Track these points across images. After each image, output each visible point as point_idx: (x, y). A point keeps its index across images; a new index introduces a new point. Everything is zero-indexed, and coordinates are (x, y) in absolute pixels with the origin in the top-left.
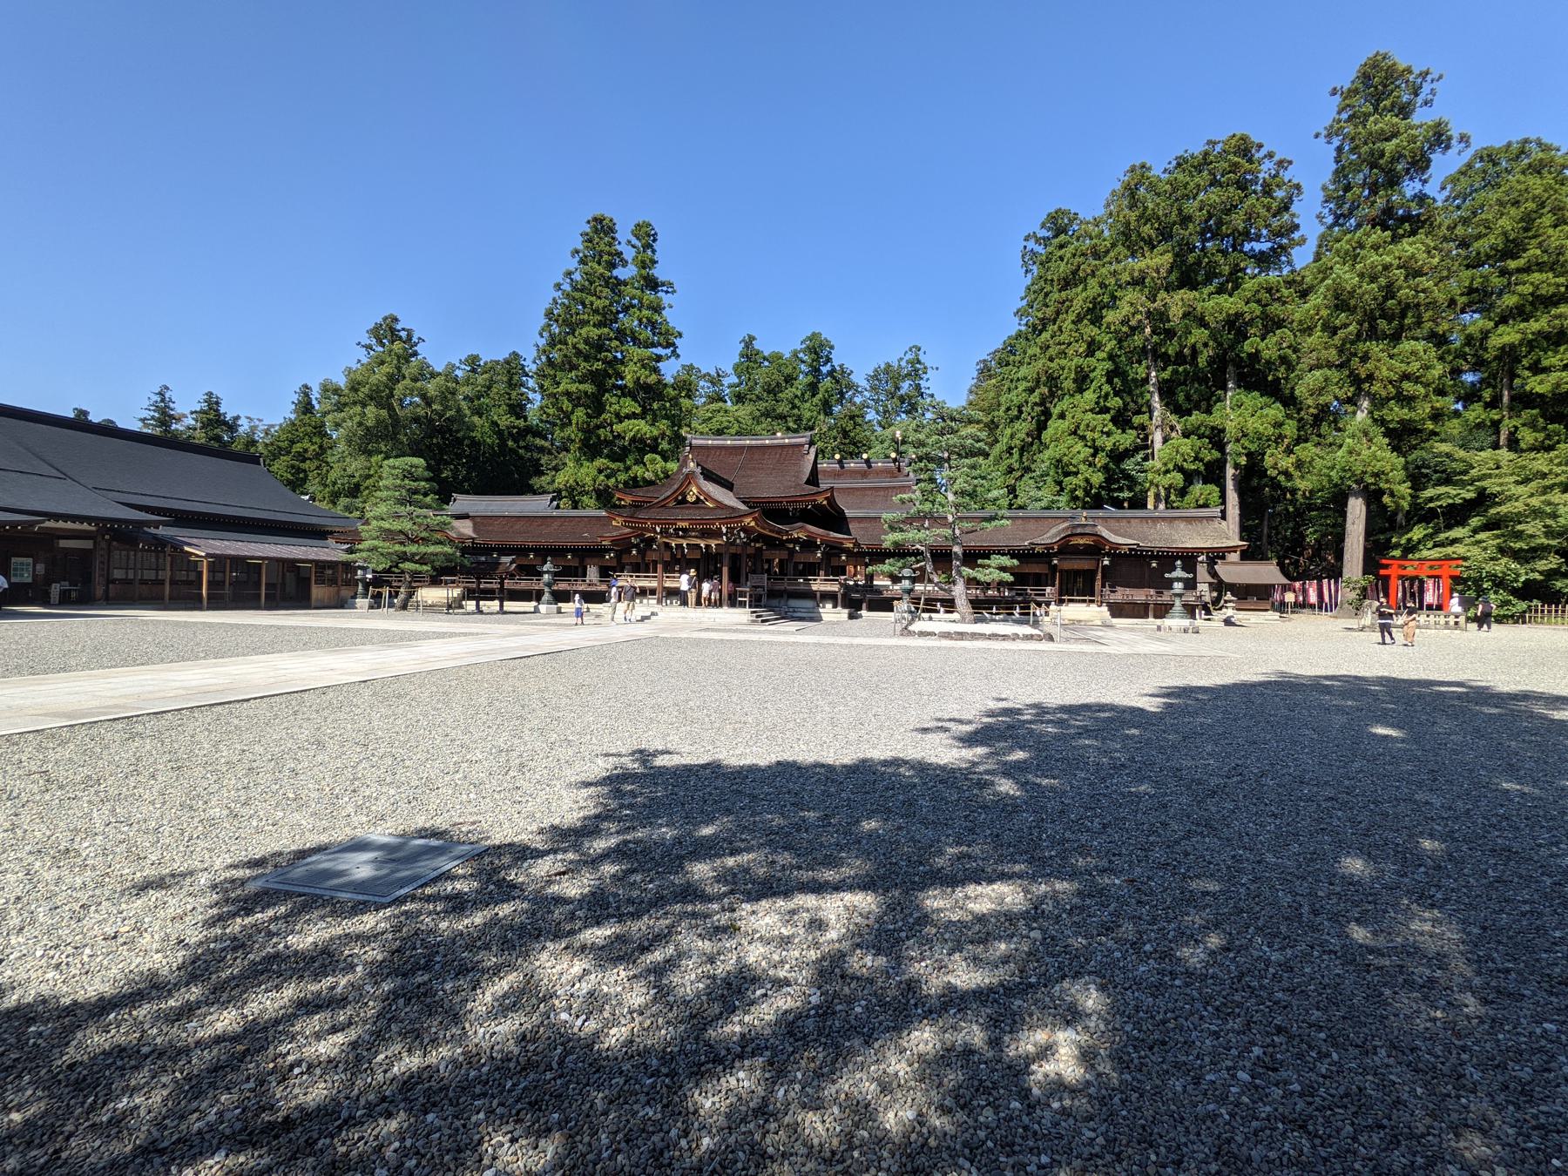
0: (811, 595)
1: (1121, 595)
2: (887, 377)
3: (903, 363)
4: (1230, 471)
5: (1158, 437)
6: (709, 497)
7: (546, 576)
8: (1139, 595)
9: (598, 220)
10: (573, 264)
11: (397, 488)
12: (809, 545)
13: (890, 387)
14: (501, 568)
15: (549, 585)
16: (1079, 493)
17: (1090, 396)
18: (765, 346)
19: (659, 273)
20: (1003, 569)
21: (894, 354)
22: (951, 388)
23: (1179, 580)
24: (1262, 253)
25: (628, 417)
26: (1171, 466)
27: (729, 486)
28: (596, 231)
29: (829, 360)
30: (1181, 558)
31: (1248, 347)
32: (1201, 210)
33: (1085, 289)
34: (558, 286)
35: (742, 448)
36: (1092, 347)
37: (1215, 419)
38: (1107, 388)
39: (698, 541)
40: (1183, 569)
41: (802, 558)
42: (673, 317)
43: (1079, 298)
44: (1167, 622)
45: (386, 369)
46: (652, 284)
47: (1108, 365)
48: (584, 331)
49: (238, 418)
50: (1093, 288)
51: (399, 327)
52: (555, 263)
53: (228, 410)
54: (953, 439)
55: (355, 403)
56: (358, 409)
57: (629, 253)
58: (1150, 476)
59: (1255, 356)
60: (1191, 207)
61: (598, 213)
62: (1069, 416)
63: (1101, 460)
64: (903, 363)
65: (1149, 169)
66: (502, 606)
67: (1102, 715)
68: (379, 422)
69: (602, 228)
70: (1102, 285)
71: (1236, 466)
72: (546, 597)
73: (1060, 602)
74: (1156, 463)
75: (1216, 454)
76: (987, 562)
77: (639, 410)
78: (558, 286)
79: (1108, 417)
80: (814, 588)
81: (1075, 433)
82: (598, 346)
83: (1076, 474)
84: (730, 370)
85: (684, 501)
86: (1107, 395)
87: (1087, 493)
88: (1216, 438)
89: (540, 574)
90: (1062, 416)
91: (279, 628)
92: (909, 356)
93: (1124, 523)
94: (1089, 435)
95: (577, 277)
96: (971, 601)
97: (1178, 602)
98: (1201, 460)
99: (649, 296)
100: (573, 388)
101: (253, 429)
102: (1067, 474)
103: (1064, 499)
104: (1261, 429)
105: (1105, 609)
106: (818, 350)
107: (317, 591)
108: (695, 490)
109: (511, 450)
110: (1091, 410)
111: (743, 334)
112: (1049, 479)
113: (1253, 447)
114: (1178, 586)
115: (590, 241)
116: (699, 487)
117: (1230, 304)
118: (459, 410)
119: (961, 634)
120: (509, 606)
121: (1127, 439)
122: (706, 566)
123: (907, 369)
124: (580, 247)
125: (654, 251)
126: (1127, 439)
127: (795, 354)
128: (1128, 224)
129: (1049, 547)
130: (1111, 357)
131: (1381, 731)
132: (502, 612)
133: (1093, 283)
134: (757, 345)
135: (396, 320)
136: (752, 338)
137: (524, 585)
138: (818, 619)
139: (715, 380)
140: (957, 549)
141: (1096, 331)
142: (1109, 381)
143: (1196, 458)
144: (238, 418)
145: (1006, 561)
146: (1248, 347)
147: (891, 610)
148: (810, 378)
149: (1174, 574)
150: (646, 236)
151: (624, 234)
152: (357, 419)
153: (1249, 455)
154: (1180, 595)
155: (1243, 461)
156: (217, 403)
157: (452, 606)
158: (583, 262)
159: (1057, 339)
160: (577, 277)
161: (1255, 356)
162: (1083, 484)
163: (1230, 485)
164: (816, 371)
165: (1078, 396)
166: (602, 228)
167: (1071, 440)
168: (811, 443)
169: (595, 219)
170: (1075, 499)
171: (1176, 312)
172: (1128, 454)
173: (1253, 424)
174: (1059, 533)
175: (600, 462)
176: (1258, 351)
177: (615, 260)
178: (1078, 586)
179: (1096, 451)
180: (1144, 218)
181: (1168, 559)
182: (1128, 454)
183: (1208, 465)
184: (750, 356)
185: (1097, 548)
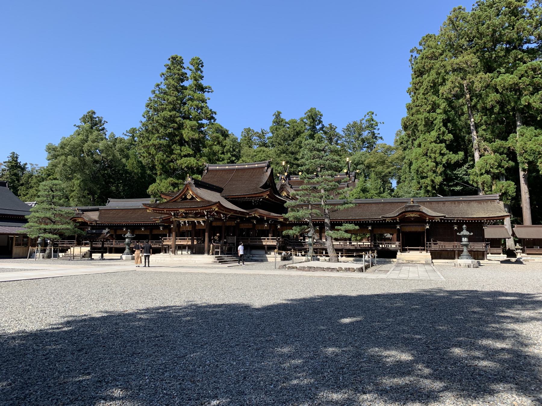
0: (262, 247)
1: (441, 245)
2: (354, 129)
3: (364, 122)
4: (522, 173)
5: (477, 155)
6: (197, 196)
7: (127, 240)
8: (449, 246)
9: (174, 58)
10: (162, 79)
11: (47, 196)
12: (261, 220)
13: (356, 135)
14: (102, 236)
15: (128, 244)
16: (429, 188)
17: (434, 134)
18: (286, 117)
19: (204, 83)
20: (347, 231)
21: (358, 116)
22: (389, 134)
23: (465, 236)
24: (533, 49)
25: (185, 156)
26: (483, 171)
27: (219, 190)
28: (173, 63)
29: (320, 122)
30: (466, 223)
31: (523, 101)
32: (488, 28)
33: (428, 76)
34: (154, 92)
35: (233, 170)
36: (434, 107)
37: (509, 144)
38: (443, 129)
39: (193, 220)
41: (259, 227)
42: (211, 105)
43: (427, 79)
44: (458, 261)
45: (80, 137)
46: (201, 88)
47: (444, 116)
48: (162, 114)
49: (26, 164)
50: (433, 75)
51: (95, 116)
53: (22, 161)
54: (319, 161)
55: (62, 155)
56: (63, 157)
57: (189, 74)
58: (471, 177)
59: (529, 106)
60: (482, 28)
61: (174, 55)
62: (422, 145)
63: (440, 169)
64: (364, 122)
65: (464, 10)
66: (102, 256)
67: (160, 311)
68: (73, 163)
69: (176, 61)
70: (438, 74)
71: (524, 170)
72: (127, 251)
73: (404, 250)
74: (476, 169)
75: (512, 163)
76: (339, 227)
77: (191, 152)
78: (154, 92)
79: (444, 145)
80: (264, 244)
81: (426, 155)
82: (172, 120)
83: (427, 177)
84: (269, 131)
85: (186, 198)
86: (444, 133)
87: (434, 188)
88: (512, 155)
89: (125, 239)
90: (419, 145)
91: (191, 273)
92: (367, 117)
93: (441, 205)
94: (433, 155)
95: (163, 87)
97: (465, 249)
98: (503, 167)
99: (198, 94)
100: (156, 143)
101: (33, 169)
102: (423, 178)
103: (422, 191)
104: (534, 148)
106: (314, 118)
107: (16, 250)
108: (191, 193)
109: (149, 175)
110: (435, 142)
111: (274, 111)
112: (414, 181)
113: (531, 159)
114: (465, 240)
115: (169, 68)
117: (509, 79)
118: (114, 156)
120: (107, 256)
121: (455, 157)
122: (195, 232)
123: (365, 124)
124: (164, 72)
125: (202, 72)
126: (455, 157)
127: (302, 120)
128: (450, 39)
129: (394, 219)
130: (445, 112)
131: (347, 320)
132: (102, 258)
133: (433, 72)
134: (282, 116)
135: (94, 113)
136: (279, 113)
137: (115, 244)
138: (267, 260)
139: (261, 135)
140: (327, 221)
141: (435, 98)
142: (445, 125)
143: (500, 166)
144: (26, 164)
145: (351, 227)
146: (523, 101)
148: (310, 132)
149: (462, 233)
150: (198, 65)
151: (187, 64)
152: (62, 162)
153: (530, 163)
154: (466, 246)
155: (526, 166)
156: (17, 158)
157: (88, 256)
158: (166, 79)
159: (415, 104)
160: (163, 87)
161: (529, 106)
162: (430, 183)
163: (522, 181)
164: (313, 128)
165: (427, 134)
166: (176, 61)
167: (424, 159)
168: (268, 166)
169: (172, 58)
170: (428, 192)
171: (478, 86)
172: (458, 165)
173: (530, 145)
175: (170, 179)
176: (529, 103)
177: (182, 78)
178: (412, 242)
179: (437, 164)
180: (459, 36)
182: (458, 165)
183: (507, 169)
184: (278, 122)
185: (422, 219)
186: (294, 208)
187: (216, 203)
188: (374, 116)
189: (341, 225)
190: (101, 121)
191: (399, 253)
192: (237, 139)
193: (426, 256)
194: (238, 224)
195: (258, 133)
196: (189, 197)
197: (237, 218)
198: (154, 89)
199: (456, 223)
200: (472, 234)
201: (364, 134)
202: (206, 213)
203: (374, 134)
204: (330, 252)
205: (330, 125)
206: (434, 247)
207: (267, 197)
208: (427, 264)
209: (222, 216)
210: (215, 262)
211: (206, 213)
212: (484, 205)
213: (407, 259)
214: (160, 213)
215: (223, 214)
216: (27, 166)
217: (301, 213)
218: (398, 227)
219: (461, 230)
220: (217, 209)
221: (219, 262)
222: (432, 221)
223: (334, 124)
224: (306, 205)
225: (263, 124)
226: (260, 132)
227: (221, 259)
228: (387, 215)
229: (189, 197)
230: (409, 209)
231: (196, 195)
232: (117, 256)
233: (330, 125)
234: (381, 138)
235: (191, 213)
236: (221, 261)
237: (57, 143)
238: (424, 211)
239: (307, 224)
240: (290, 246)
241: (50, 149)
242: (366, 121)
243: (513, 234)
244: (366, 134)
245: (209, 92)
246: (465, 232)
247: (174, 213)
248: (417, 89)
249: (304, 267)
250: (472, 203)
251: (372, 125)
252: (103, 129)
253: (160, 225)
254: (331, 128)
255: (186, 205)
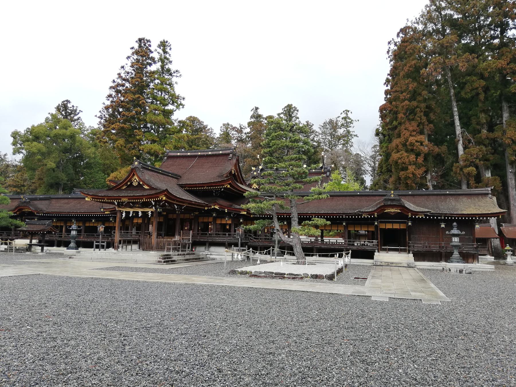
9: (140, 40)
18: (264, 112)
19: (172, 67)
20: (316, 227)
40: (458, 228)
52: (114, 64)
57: (155, 55)
84: (247, 126)
92: (344, 115)
96: (302, 248)
105: (411, 255)
114: (456, 240)
116: (138, 177)
119: (136, 268)
123: (341, 122)
129: (371, 213)
136: (257, 109)
139: (240, 131)
145: (321, 221)
147: (372, 258)
150: (163, 45)
151: (154, 47)
174: (377, 205)
178: (393, 241)
181: (450, 220)
185: (404, 214)
186: (255, 198)
187: (164, 191)
188: (349, 115)
189: (310, 219)
190: (76, 111)
191: (376, 254)
192: (179, 106)
193: (407, 258)
194: (197, 217)
195: (237, 128)
196: (135, 184)
197: (195, 210)
198: (119, 72)
199: (444, 221)
200: (464, 233)
201: (339, 130)
202: (153, 203)
203: (349, 132)
204: (298, 249)
205: (307, 122)
206: (419, 246)
207: (229, 186)
208: (409, 266)
209: (176, 207)
210: (159, 262)
211: (153, 203)
212: (476, 200)
213: (386, 261)
214: (101, 202)
215: (177, 205)
216: (6, 157)
217: (265, 205)
218: (376, 223)
219: (449, 227)
220: (164, 198)
221: (164, 262)
222: (415, 217)
223: (311, 122)
224: (271, 195)
225: (242, 119)
226: (238, 127)
227: (168, 258)
228: (363, 210)
229: (135, 184)
230: (389, 203)
231: (143, 181)
232: (63, 250)
233: (307, 122)
234: (356, 136)
235: (137, 203)
236: (168, 260)
237: (22, 130)
238: (406, 205)
239: (271, 218)
240: (259, 243)
241: (15, 135)
242: (342, 119)
243: (501, 233)
244: (341, 131)
245: (177, 76)
246: (455, 231)
247: (118, 203)
248: (396, 75)
249: (261, 273)
250: (461, 197)
251: (347, 121)
252: (78, 119)
253: (110, 217)
254: (308, 125)
255: (130, 193)
